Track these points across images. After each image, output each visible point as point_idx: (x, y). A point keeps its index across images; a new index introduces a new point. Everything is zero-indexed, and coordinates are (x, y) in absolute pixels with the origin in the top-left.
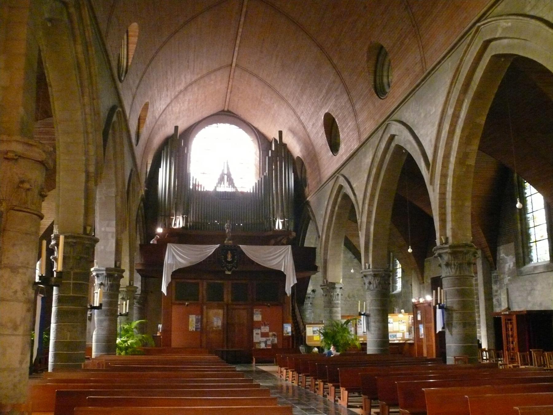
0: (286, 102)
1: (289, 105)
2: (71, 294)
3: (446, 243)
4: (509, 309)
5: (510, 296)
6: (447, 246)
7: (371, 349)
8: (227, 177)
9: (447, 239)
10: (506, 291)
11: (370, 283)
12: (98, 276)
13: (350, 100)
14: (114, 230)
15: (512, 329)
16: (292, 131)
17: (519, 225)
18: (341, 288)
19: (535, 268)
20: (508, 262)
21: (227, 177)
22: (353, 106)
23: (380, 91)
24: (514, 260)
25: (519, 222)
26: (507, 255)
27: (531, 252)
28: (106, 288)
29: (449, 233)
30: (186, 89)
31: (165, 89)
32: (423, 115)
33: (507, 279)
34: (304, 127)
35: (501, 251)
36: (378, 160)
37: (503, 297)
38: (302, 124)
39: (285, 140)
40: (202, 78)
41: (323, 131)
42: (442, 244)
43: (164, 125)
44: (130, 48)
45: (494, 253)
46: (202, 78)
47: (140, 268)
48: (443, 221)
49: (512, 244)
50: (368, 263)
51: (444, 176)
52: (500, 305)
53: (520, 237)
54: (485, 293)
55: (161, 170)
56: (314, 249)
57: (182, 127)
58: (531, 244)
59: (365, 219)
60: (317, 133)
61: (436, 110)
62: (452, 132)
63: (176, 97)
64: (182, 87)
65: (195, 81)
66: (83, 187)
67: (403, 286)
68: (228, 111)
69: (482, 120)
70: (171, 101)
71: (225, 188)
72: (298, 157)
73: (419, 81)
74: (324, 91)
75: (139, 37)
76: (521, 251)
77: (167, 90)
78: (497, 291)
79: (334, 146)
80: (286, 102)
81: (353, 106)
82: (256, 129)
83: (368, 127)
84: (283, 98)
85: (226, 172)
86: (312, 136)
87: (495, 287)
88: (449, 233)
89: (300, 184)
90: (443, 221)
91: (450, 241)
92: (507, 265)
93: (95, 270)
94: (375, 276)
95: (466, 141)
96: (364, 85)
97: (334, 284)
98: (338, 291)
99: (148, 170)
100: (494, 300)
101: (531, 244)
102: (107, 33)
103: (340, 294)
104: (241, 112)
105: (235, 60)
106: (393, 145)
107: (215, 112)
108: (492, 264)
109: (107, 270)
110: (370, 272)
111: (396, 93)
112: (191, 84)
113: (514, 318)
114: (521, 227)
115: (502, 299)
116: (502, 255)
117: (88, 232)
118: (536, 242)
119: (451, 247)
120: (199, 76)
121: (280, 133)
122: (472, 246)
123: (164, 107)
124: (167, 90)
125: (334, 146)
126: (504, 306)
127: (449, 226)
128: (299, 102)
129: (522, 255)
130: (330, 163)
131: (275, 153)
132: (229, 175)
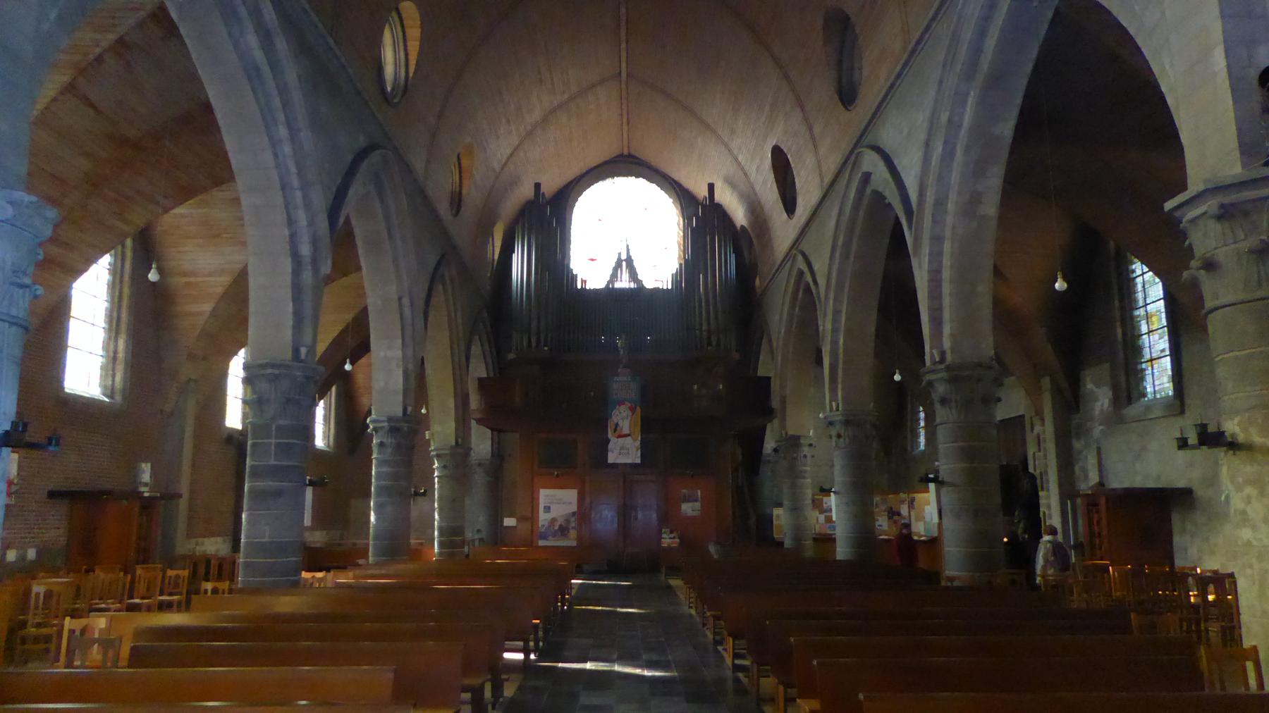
0: (714, 132)
1: (719, 137)
2: (272, 462)
3: (942, 360)
4: (1101, 484)
5: (1103, 456)
6: (942, 366)
7: (842, 551)
8: (626, 263)
9: (943, 354)
10: (1095, 453)
11: (839, 436)
12: (375, 429)
13: (806, 119)
14: (399, 353)
15: (1098, 523)
16: (730, 182)
17: (1119, 331)
18: (811, 445)
19: (1148, 408)
20: (1100, 399)
21: (626, 263)
22: (811, 129)
23: (847, 96)
24: (1110, 394)
25: (1118, 324)
26: (1098, 386)
27: (1143, 379)
28: (389, 450)
29: (947, 344)
30: (545, 120)
31: (504, 121)
32: (906, 131)
33: (1097, 430)
34: (746, 174)
35: (1088, 379)
36: (845, 218)
37: (1092, 462)
38: (743, 169)
39: (718, 197)
40: (571, 99)
41: (771, 176)
42: (934, 363)
43: (515, 182)
44: (409, 48)
45: (1075, 382)
46: (571, 99)
47: (478, 416)
48: (937, 322)
49: (1106, 366)
50: (836, 400)
51: (937, 239)
52: (1086, 477)
53: (1121, 355)
54: (1058, 456)
55: (515, 257)
56: (769, 378)
57: (550, 185)
58: (1144, 366)
59: (829, 326)
60: (765, 182)
61: (921, 118)
62: (948, 155)
63: (529, 134)
64: (537, 115)
65: (559, 107)
66: (288, 279)
67: (927, 444)
68: (630, 156)
69: (1006, 129)
70: (521, 143)
71: (624, 283)
72: (742, 227)
73: (899, 68)
74: (767, 108)
75: (422, 27)
76: (1123, 378)
77: (508, 121)
78: (1080, 452)
79: (789, 204)
80: (714, 132)
81: (811, 129)
82: (676, 182)
83: (832, 163)
84: (708, 126)
85: (624, 257)
86: (758, 188)
87: (1077, 445)
88: (947, 344)
89: (746, 272)
90: (937, 322)
91: (949, 358)
92: (1099, 404)
93: (374, 421)
94: (847, 423)
95: (978, 170)
96: (823, 90)
97: (799, 437)
98: (806, 450)
99: (496, 257)
100: (1077, 469)
101: (1144, 366)
102: (1224, 234)
103: (809, 455)
104: (648, 152)
105: (624, 65)
106: (868, 191)
107: (603, 159)
108: (1070, 403)
109: (390, 419)
110: (838, 417)
111: (869, 96)
112: (553, 111)
113: (1103, 502)
114: (1124, 334)
115: (1090, 467)
116: (1090, 386)
117: (303, 357)
118: (1152, 360)
119: (948, 368)
120: (566, 96)
121: (711, 187)
122: (990, 368)
123: (508, 151)
124: (508, 121)
125: (789, 204)
126: (1094, 478)
127: (947, 330)
128: (733, 132)
129: (1124, 385)
130: (784, 231)
131: (704, 220)
132: (629, 261)
